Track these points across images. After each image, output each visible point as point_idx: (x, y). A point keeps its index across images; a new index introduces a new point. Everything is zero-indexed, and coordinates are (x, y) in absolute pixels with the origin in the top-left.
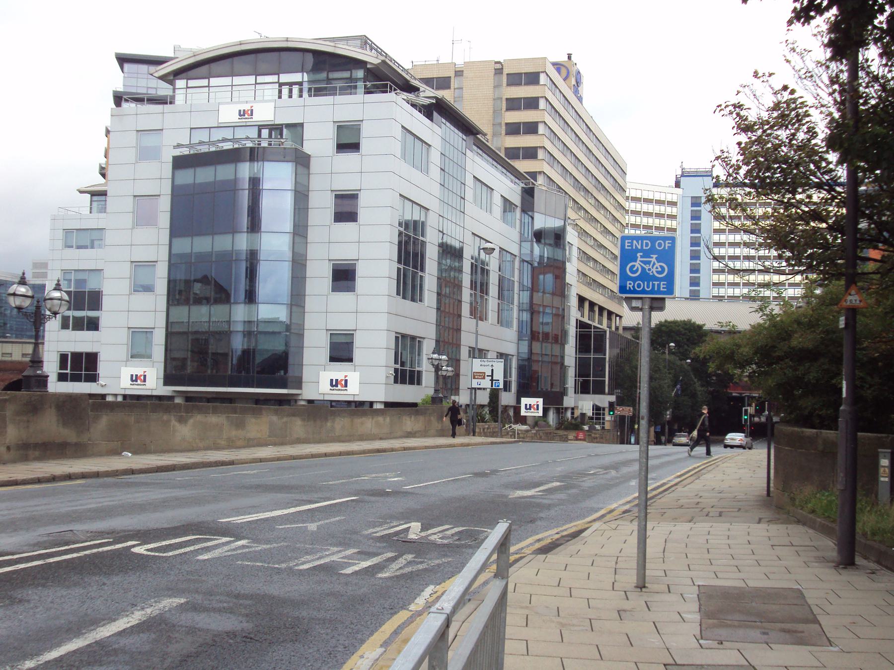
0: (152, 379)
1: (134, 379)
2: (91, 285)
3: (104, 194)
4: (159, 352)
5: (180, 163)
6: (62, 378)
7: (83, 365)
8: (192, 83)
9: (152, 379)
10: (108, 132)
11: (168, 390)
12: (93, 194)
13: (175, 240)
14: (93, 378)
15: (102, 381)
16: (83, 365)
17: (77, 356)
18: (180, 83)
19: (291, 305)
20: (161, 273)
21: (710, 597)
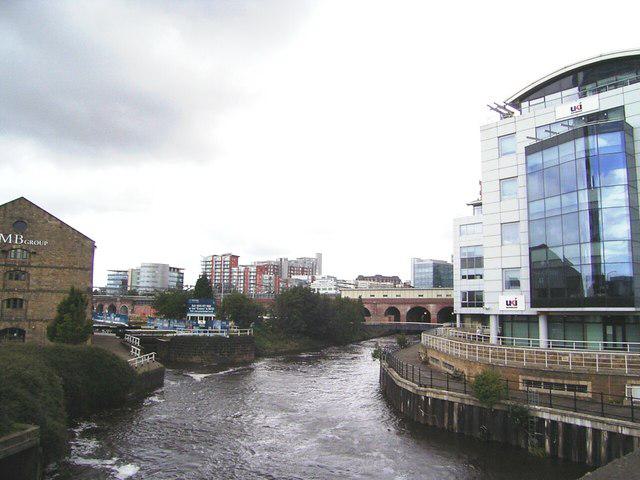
0: (521, 302)
1: (509, 303)
2: (478, 253)
3: (481, 204)
4: (525, 285)
5: (530, 151)
6: (464, 305)
7: (474, 299)
8: (532, 103)
9: (521, 302)
10: (480, 183)
11: (533, 311)
12: (475, 205)
13: (529, 157)
14: (481, 305)
15: (486, 306)
16: (474, 299)
17: (471, 293)
18: (524, 105)
19: (632, 240)
20: (524, 277)
21: (420, 266)
